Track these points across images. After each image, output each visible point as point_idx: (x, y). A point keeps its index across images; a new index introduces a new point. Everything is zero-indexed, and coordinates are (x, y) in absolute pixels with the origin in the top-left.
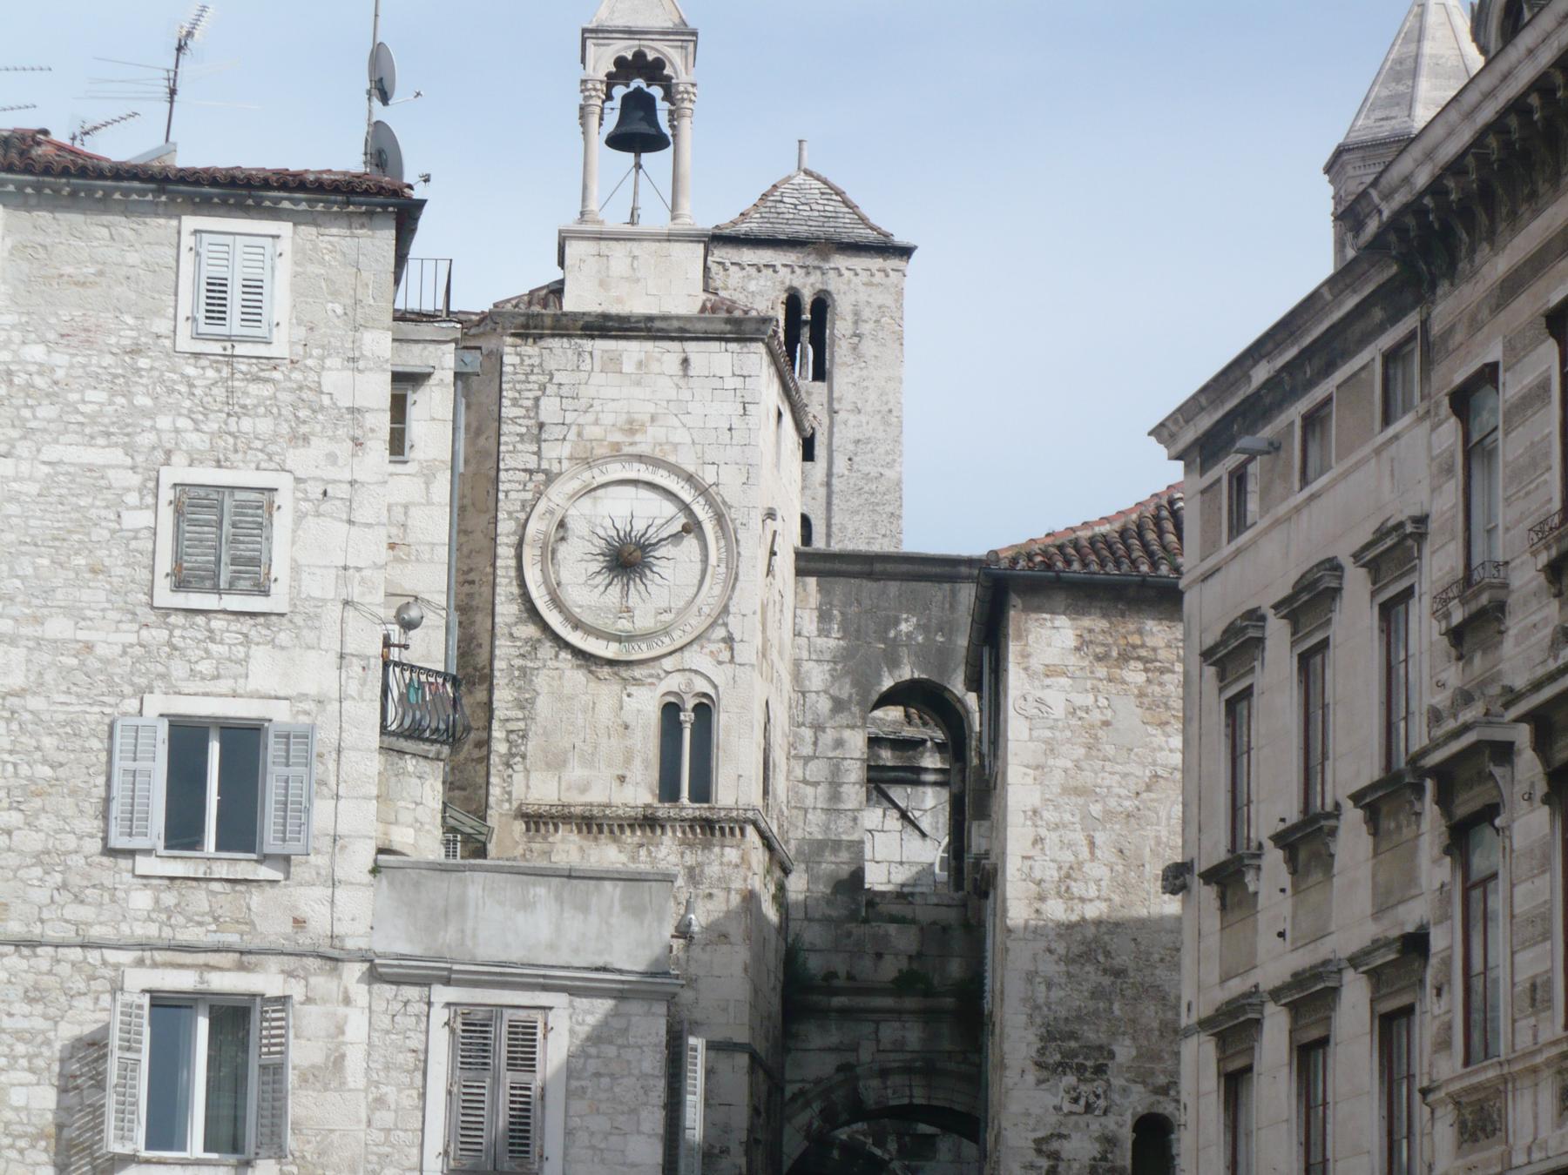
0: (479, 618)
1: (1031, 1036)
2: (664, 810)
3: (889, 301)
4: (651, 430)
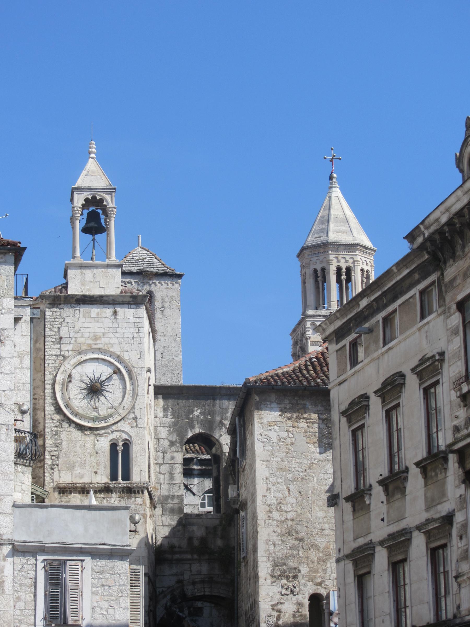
0: (39, 412)
2: (112, 484)
4: (103, 339)
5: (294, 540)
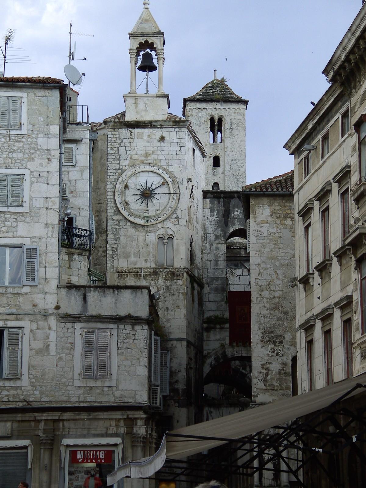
1: (259, 333)
3: (240, 117)
5: (280, 313)
